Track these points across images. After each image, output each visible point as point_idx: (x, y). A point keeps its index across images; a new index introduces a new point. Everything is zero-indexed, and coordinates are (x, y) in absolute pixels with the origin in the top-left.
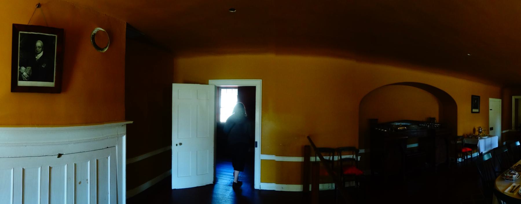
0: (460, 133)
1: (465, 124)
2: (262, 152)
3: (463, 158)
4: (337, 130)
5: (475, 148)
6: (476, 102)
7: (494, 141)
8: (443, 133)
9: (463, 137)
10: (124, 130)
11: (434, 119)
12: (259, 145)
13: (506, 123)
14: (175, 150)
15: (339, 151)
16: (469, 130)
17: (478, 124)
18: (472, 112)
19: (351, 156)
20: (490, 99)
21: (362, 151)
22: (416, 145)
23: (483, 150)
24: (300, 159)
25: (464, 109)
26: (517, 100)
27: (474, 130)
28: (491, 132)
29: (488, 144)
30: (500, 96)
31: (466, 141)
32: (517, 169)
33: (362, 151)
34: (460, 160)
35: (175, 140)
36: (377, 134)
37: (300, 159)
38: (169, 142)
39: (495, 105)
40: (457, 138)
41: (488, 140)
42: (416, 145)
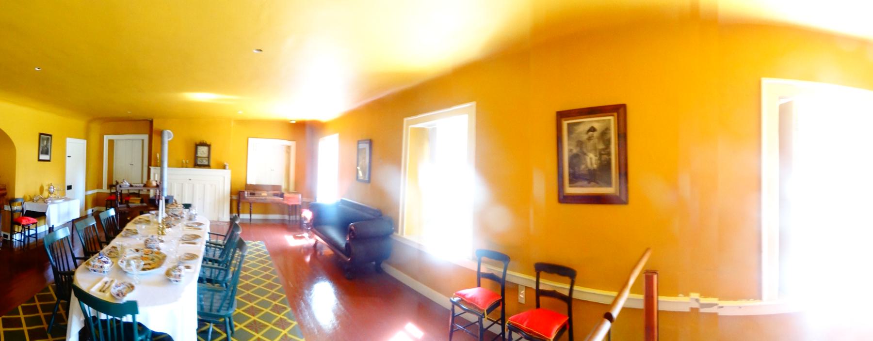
0: (19, 194)
5: (41, 215)
6: (44, 144)
9: (24, 199)
16: (33, 190)
18: (565, 199)
20: (69, 140)
26: (111, 142)
30: (87, 137)
31: (29, 207)
32: (110, 255)
34: (17, 237)
39: (75, 150)
40: (12, 201)
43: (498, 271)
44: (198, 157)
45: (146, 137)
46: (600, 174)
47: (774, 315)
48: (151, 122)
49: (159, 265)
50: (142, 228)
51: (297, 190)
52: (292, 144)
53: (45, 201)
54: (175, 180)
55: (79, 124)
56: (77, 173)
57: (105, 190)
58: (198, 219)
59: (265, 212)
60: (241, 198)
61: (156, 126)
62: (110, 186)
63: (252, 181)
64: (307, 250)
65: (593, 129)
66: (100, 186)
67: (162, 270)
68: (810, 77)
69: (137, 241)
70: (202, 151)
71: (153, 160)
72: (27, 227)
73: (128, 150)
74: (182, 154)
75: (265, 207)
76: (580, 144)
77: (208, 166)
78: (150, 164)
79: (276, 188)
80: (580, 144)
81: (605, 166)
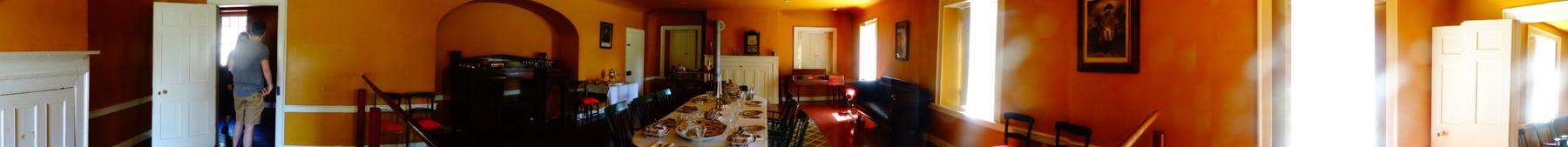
0: (582, 77)
1: (590, 64)
2: (287, 103)
3: (585, 112)
4: (409, 70)
5: (603, 98)
6: (606, 32)
7: (633, 90)
8: (556, 75)
9: (586, 83)
10: (86, 65)
11: (544, 55)
12: (282, 91)
13: (651, 66)
14: (157, 101)
15: (408, 97)
16: (595, 74)
17: (610, 64)
18: (1084, 68)
19: (424, 106)
20: (629, 30)
21: (439, 98)
22: (517, 92)
23: (614, 101)
24: (352, 109)
25: (588, 40)
26: (668, 33)
27: (603, 74)
28: (628, 78)
29: (623, 94)
30: (645, 27)
31: (590, 89)
32: (665, 123)
33: (439, 98)
34: (581, 116)
35: (157, 84)
36: (464, 77)
37: (352, 109)
38: (149, 91)
39: (634, 38)
40: (577, 83)
41: (623, 88)
42: (517, 92)
43: (1024, 131)
44: (747, 44)
45: (699, 28)
46: (1115, 46)
47: (32, 47)
48: (704, 13)
49: (720, 133)
50: (700, 105)
51: (840, 73)
52: (834, 30)
53: (606, 84)
54: (730, 68)
55: (638, 15)
56: (636, 61)
57: (662, 76)
58: (756, 98)
59: (812, 94)
60: (790, 81)
61: (709, 16)
62: (666, 73)
63: (798, 65)
64: (850, 124)
65: (1110, 6)
66: (657, 73)
67: (723, 137)
68: (963, 93)
69: (699, 115)
70: (752, 40)
71: (708, 48)
72: (589, 108)
73: (683, 40)
74: (732, 44)
75: (812, 90)
76: (1098, 19)
77: (758, 54)
78: (703, 53)
79: (822, 71)
80: (1098, 19)
81: (1119, 37)
